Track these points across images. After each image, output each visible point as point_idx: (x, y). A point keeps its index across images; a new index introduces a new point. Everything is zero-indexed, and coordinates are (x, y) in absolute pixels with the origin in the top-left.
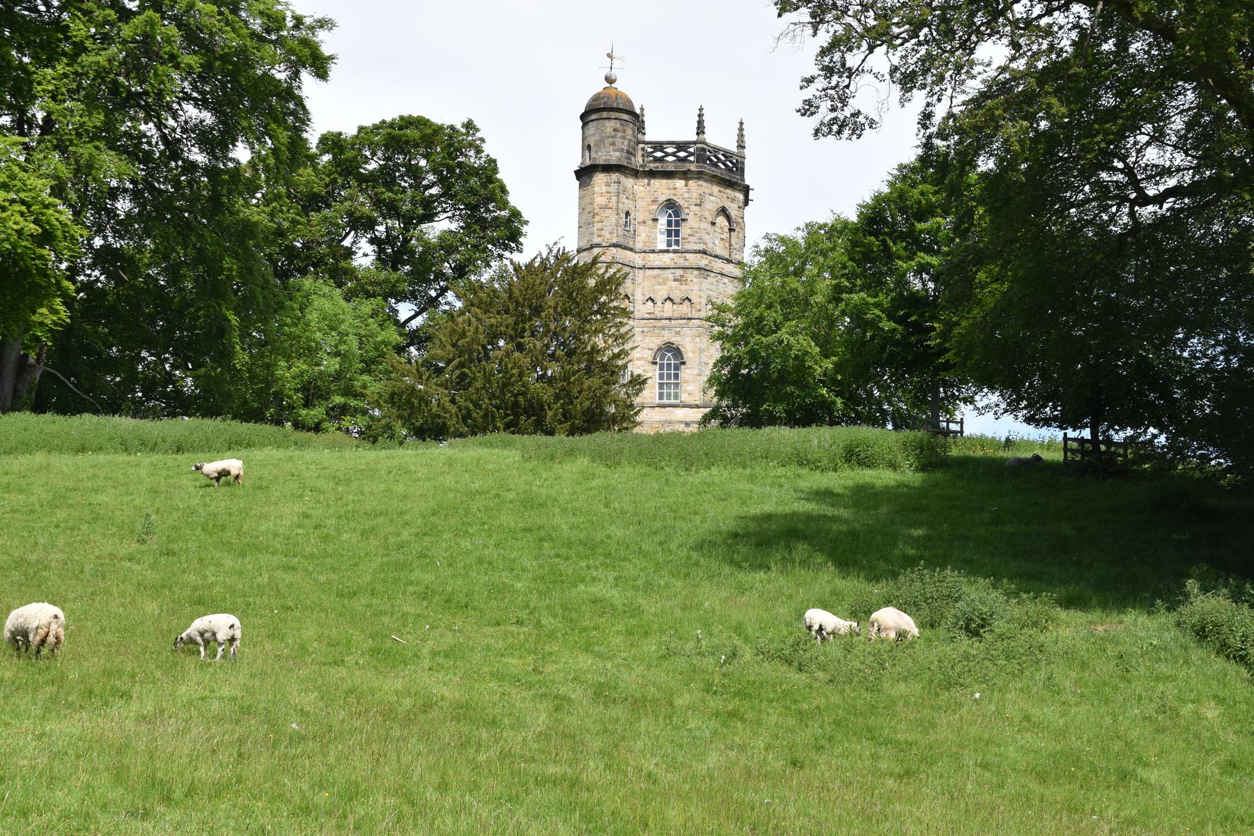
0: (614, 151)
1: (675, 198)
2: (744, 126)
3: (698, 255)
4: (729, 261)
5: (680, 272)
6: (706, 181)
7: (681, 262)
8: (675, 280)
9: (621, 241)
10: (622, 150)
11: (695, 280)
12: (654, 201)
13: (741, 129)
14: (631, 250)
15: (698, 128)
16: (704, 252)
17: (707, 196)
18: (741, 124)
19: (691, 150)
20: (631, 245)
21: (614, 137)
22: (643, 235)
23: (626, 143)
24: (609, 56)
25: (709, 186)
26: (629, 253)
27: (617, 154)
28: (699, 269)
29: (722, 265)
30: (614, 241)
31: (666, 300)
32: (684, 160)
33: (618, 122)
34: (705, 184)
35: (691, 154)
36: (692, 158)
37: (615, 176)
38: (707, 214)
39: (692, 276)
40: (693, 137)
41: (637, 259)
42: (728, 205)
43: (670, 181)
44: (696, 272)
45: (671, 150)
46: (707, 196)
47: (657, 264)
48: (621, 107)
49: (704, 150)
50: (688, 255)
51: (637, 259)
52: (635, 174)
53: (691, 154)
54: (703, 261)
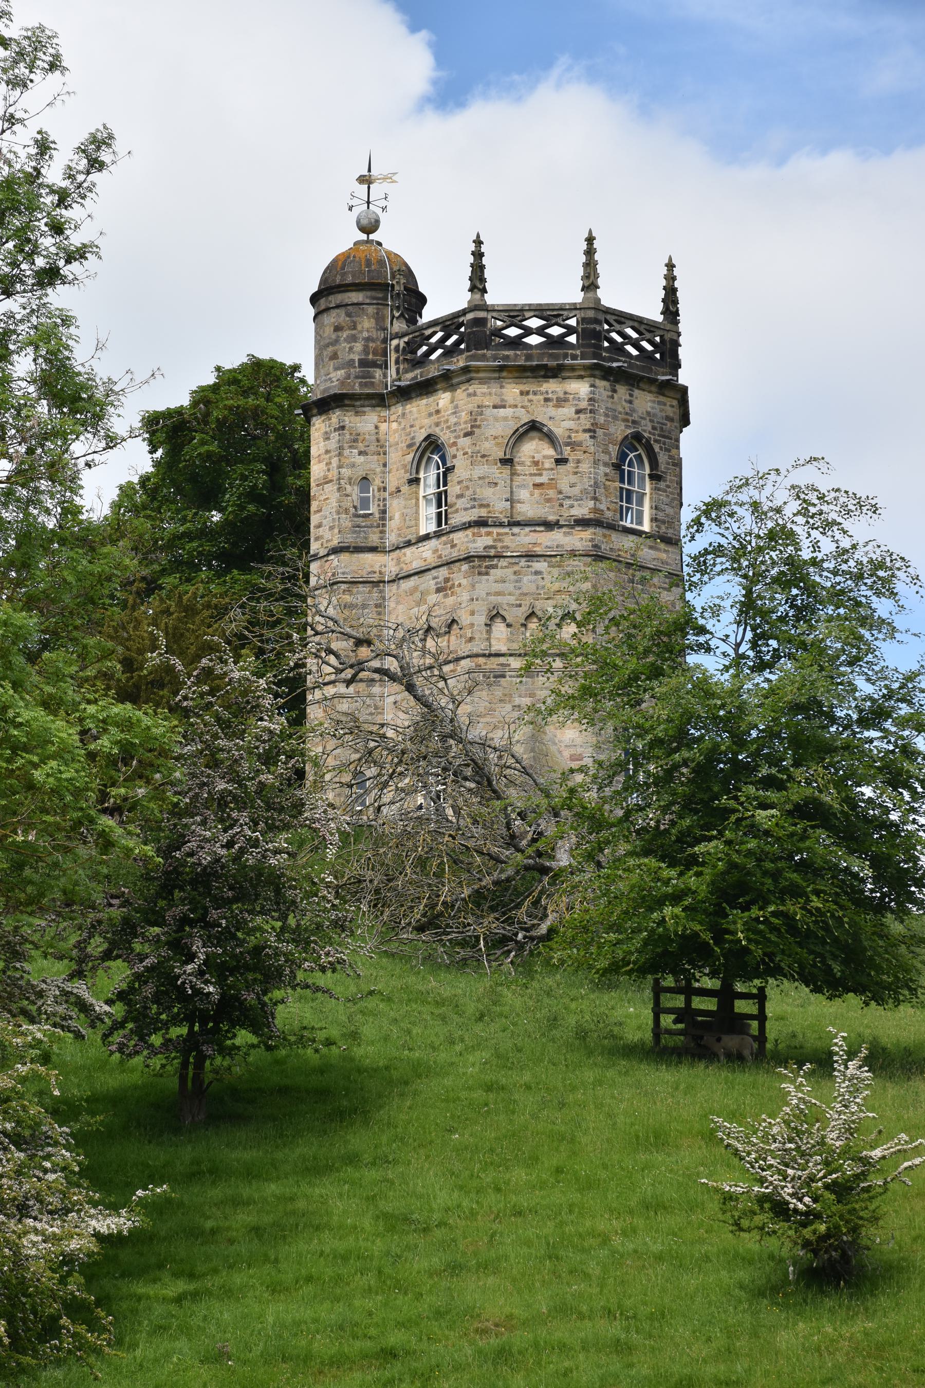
0: (336, 369)
1: (437, 430)
2: (596, 244)
3: (469, 532)
4: (549, 526)
5: (443, 572)
6: (483, 381)
7: (448, 553)
8: (438, 590)
9: (350, 539)
10: (351, 363)
11: (464, 582)
12: (409, 446)
13: (590, 252)
14: (373, 549)
15: (586, 277)
16: (481, 523)
17: (489, 412)
18: (590, 240)
19: (573, 322)
20: (374, 539)
21: (336, 342)
22: (397, 516)
23: (358, 347)
24: (366, 180)
25: (494, 388)
26: (369, 557)
27: (341, 373)
28: (468, 559)
29: (533, 538)
30: (335, 543)
31: (492, 618)
32: (559, 342)
33: (342, 312)
34: (482, 389)
35: (570, 330)
36: (572, 339)
37: (336, 417)
38: (487, 446)
39: (460, 575)
40: (576, 296)
41: (387, 564)
42: (542, 415)
43: (431, 399)
44: (465, 567)
45: (534, 323)
46: (489, 412)
47: (416, 565)
48: (349, 279)
49: (481, 322)
50: (458, 537)
51: (387, 564)
52: (380, 401)
53: (570, 330)
54: (480, 542)
